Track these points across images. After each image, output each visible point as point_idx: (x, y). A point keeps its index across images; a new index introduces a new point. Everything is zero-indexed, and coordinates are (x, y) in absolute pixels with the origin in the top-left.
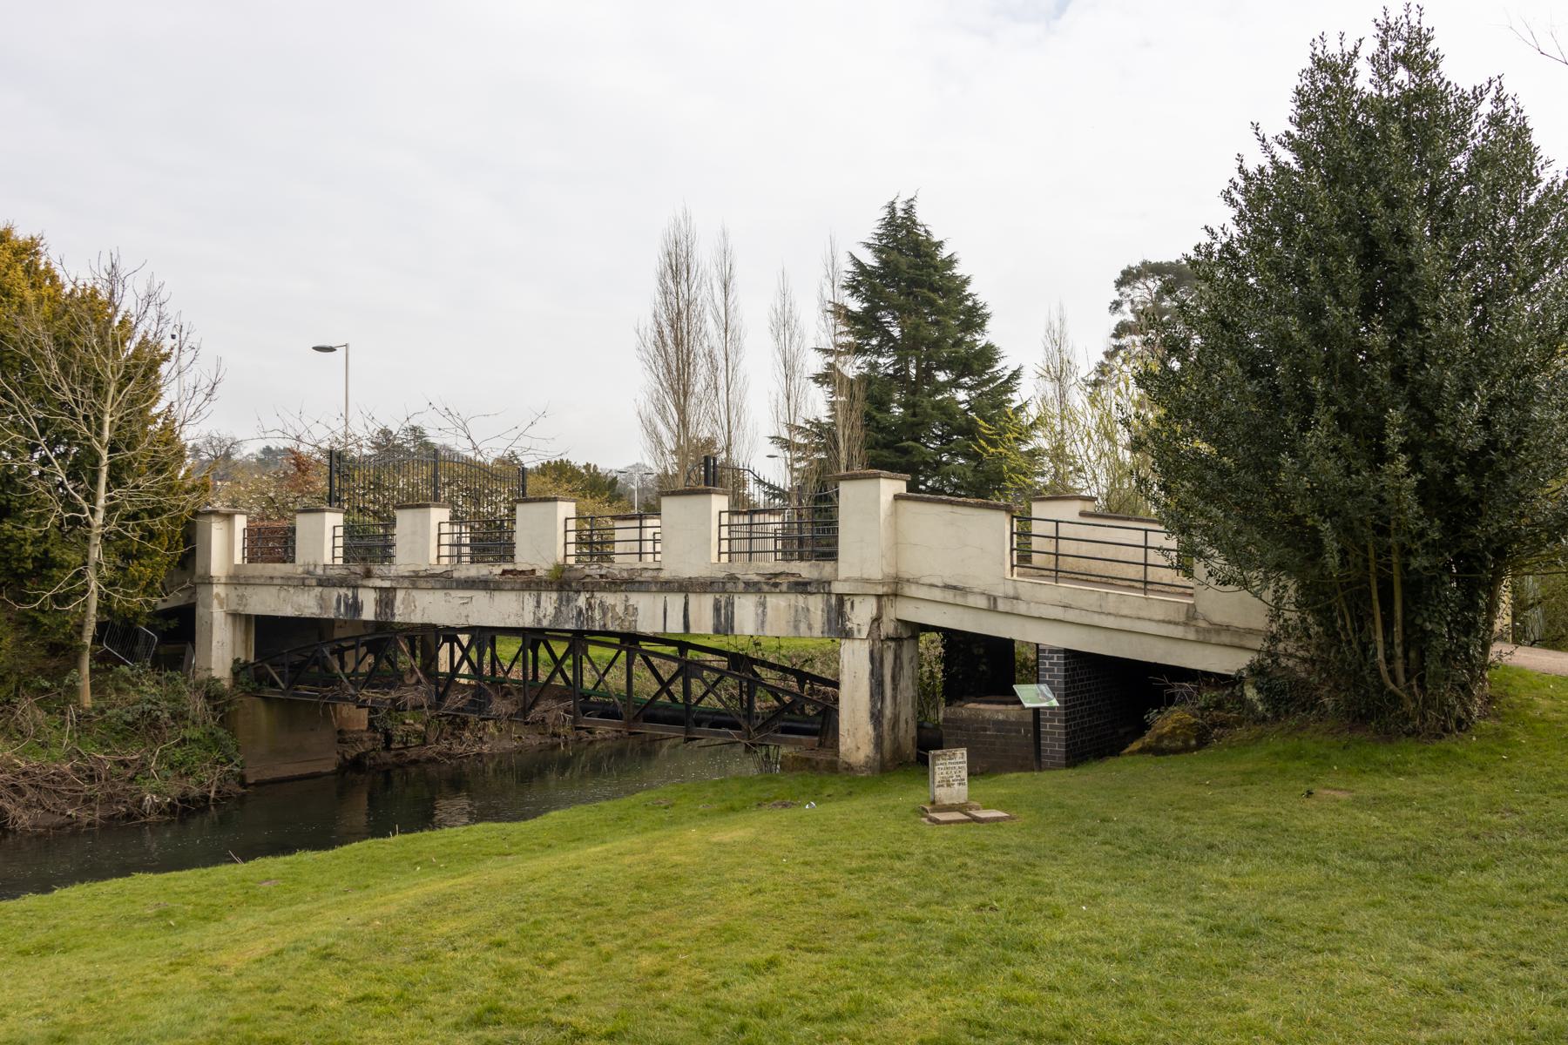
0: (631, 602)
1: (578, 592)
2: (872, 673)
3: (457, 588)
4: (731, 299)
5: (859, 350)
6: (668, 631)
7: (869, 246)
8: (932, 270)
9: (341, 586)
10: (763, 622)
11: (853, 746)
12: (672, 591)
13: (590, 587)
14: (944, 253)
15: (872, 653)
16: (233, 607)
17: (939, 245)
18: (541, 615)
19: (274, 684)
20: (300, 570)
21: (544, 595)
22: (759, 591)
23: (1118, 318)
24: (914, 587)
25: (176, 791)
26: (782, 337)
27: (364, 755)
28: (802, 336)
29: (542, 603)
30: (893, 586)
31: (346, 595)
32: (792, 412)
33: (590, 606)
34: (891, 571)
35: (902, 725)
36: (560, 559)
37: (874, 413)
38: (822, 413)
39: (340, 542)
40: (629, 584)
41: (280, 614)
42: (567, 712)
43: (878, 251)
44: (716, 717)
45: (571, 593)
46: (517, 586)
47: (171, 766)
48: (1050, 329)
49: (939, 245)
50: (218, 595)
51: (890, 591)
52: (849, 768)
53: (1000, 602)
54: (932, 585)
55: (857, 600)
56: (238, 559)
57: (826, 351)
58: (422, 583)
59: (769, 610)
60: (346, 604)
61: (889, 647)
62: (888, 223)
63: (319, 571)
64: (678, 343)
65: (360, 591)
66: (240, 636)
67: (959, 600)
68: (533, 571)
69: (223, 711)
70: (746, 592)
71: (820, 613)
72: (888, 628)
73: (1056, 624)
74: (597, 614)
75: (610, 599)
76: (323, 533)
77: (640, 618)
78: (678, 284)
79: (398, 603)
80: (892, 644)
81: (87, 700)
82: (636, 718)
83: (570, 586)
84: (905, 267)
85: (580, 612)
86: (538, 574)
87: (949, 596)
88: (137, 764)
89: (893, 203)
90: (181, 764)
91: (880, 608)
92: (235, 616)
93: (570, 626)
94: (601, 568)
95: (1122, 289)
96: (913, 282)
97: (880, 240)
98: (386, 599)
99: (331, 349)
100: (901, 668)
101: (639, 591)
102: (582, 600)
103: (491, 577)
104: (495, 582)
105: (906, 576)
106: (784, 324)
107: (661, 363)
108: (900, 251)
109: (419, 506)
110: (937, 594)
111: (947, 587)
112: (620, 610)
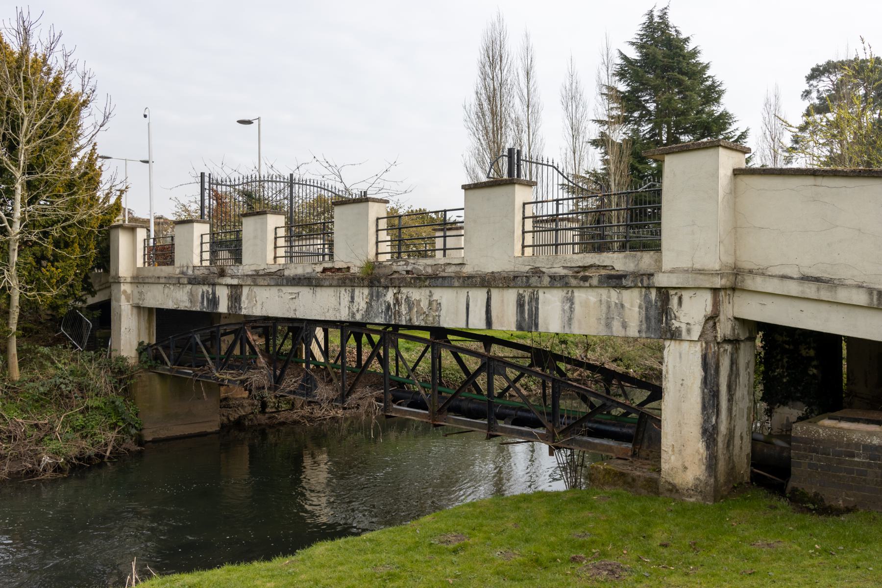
0: (435, 297)
1: (386, 287)
2: (705, 381)
3: (287, 285)
4: (531, 83)
5: (626, 120)
6: (470, 326)
7: (633, 44)
8: (681, 59)
9: (204, 284)
10: (570, 319)
11: (679, 464)
12: (474, 286)
13: (397, 283)
14: (690, 47)
15: (705, 358)
16: (136, 301)
17: (687, 40)
18: (355, 310)
19: (164, 363)
20: (178, 271)
21: (357, 291)
22: (566, 285)
23: (806, 104)
24: (759, 279)
25: (74, 451)
26: (570, 108)
27: (245, 417)
28: (585, 107)
29: (356, 299)
30: (732, 278)
31: (208, 292)
32: (577, 162)
33: (397, 302)
34: (729, 260)
35: (737, 441)
36: (371, 256)
37: (637, 165)
38: (599, 167)
39: (207, 247)
40: (434, 280)
41: (165, 307)
42: (379, 400)
43: (640, 47)
44: (519, 413)
45: (381, 289)
46: (335, 283)
47: (74, 429)
48: (767, 104)
49: (687, 40)
50: (125, 292)
51: (728, 284)
52: (673, 489)
55: (686, 295)
56: (140, 263)
57: (601, 122)
58: (260, 281)
59: (577, 306)
60: (208, 299)
61: (726, 351)
62: (648, 26)
63: (190, 272)
64: (493, 113)
65: (217, 288)
66: (144, 324)
67: (825, 295)
68: (348, 268)
69: (125, 384)
70: (552, 286)
71: (637, 309)
72: (725, 329)
74: (404, 309)
75: (416, 294)
76: (192, 240)
77: (443, 313)
78: (493, 71)
79: (244, 298)
80: (728, 347)
81: (16, 373)
82: (440, 411)
83: (379, 282)
84: (660, 57)
85: (388, 307)
86: (352, 271)
87: (810, 290)
88: (47, 428)
89: (652, 11)
90: (83, 427)
91: (716, 304)
92: (139, 308)
93: (380, 320)
94: (407, 264)
95: (811, 82)
96: (666, 68)
97: (642, 40)
98: (235, 298)
99: (249, 122)
101: (442, 286)
102: (389, 296)
103: (314, 274)
104: (317, 279)
105: (747, 266)
106: (572, 98)
107: (481, 128)
108: (656, 46)
109: (258, 214)
110: (793, 288)
111: (805, 279)
112: (424, 305)
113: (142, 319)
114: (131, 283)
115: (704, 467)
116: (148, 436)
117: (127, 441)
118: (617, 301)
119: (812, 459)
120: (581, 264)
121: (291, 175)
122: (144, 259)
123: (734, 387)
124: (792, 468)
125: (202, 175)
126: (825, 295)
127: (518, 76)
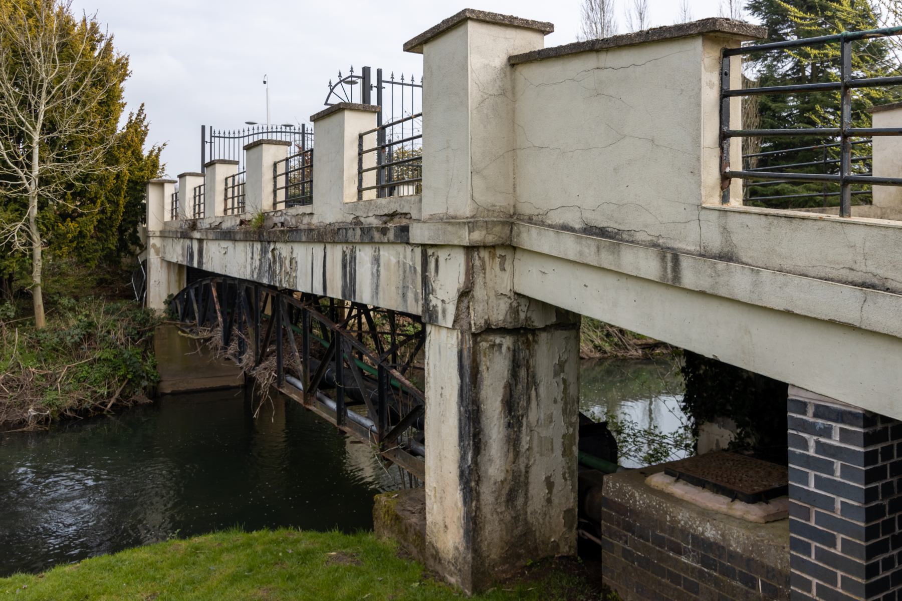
35: (537, 490)
37: (770, 104)
50: (154, 245)
53: (686, 263)
54: (566, 228)
55: (442, 254)
67: (606, 259)
73: (835, 338)
87: (587, 249)
91: (470, 272)
100: (532, 382)
105: (526, 210)
111: (592, 231)
113: (172, 273)
114: (160, 237)
115: (462, 531)
116: (167, 387)
117: (137, 393)
118: (411, 264)
119: (626, 542)
120: (386, 212)
121: (303, 126)
122: (172, 213)
123: (523, 403)
124: (603, 550)
125: (203, 128)
126: (606, 259)
127: (630, 18)
